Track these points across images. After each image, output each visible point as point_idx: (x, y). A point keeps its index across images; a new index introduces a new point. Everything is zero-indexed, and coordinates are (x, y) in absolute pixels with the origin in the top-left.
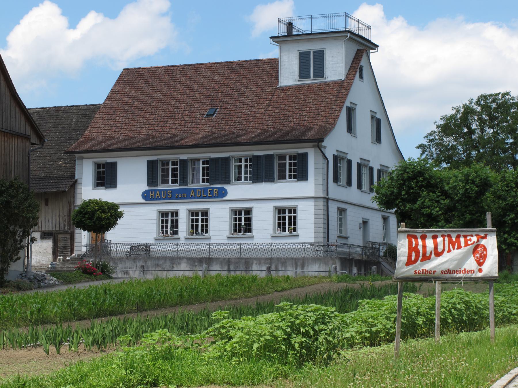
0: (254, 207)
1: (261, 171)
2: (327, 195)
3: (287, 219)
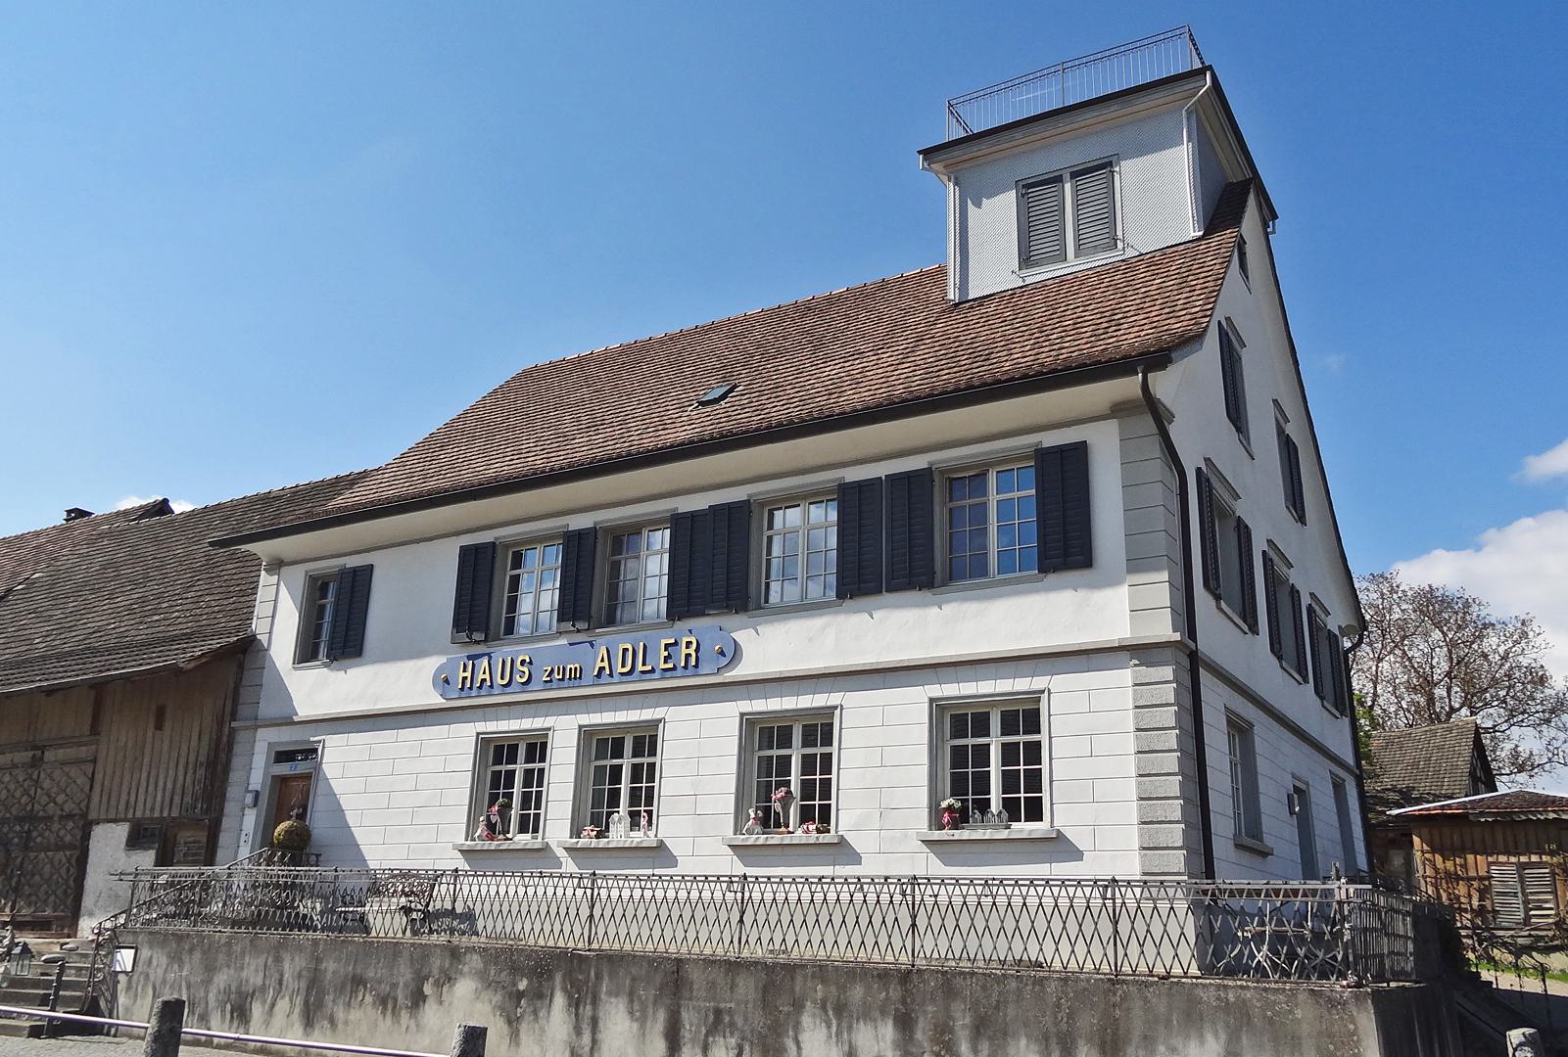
0: (122, 855)
1: (897, 544)
2: (1192, 633)
3: (988, 763)
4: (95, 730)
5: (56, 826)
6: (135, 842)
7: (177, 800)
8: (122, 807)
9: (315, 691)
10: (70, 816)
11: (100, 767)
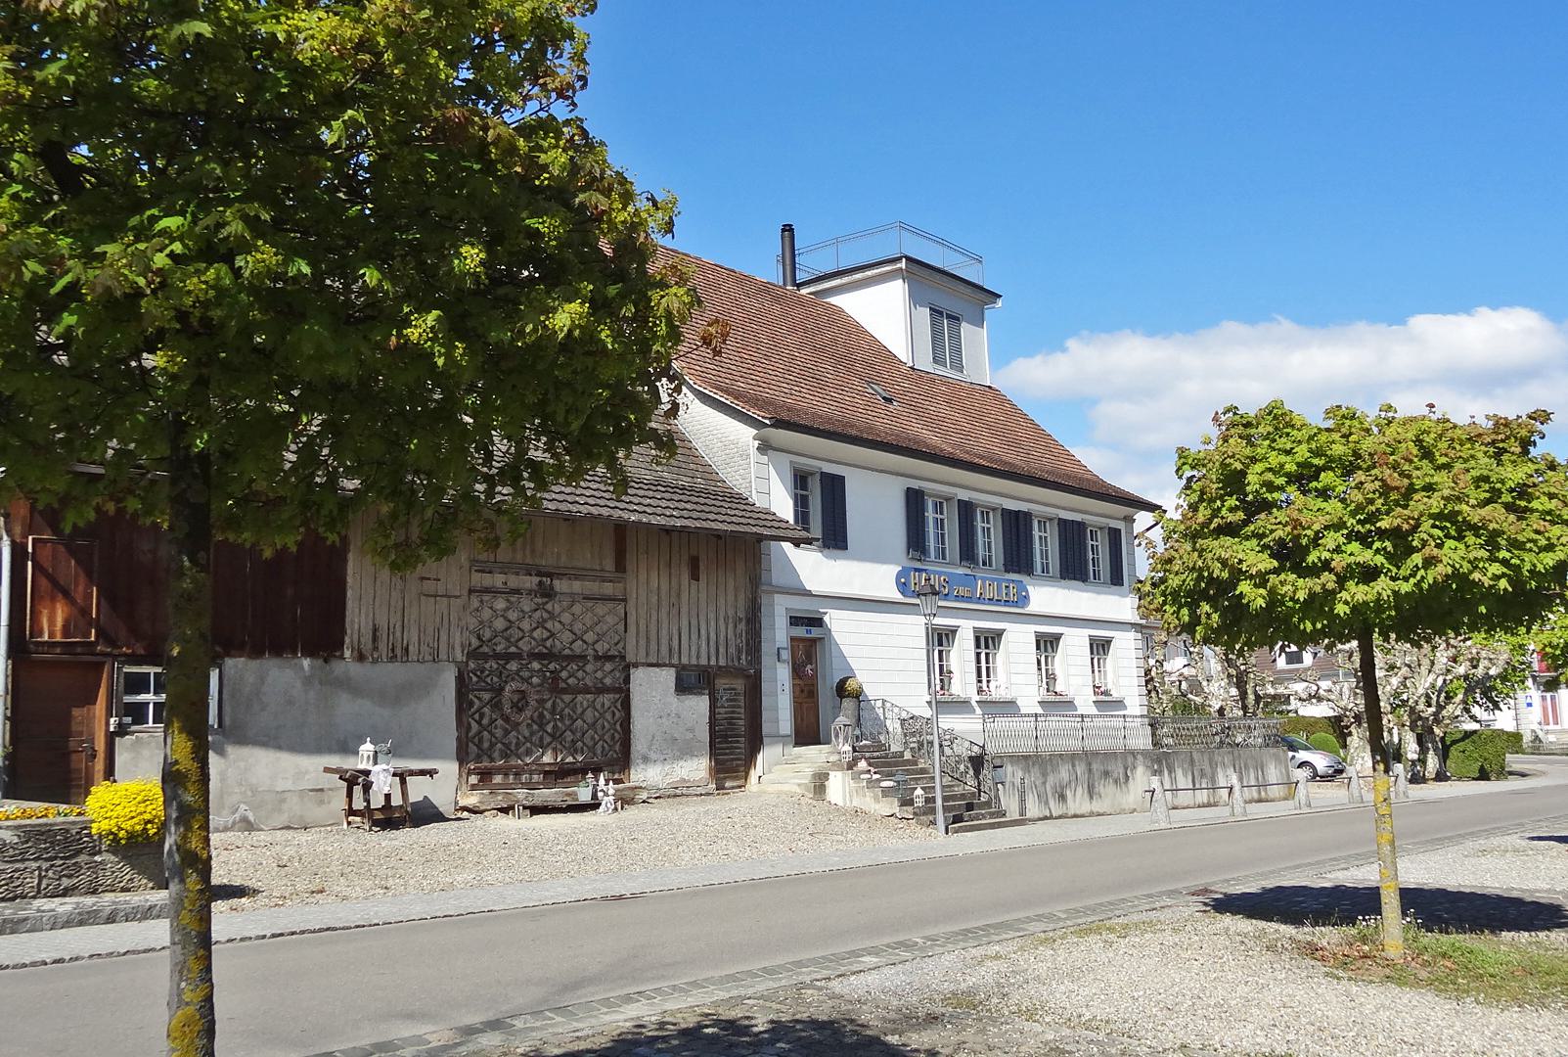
4: (620, 566)
5: (589, 668)
6: (683, 688)
7: (722, 650)
8: (664, 650)
9: (814, 569)
10: (608, 658)
11: (631, 604)
